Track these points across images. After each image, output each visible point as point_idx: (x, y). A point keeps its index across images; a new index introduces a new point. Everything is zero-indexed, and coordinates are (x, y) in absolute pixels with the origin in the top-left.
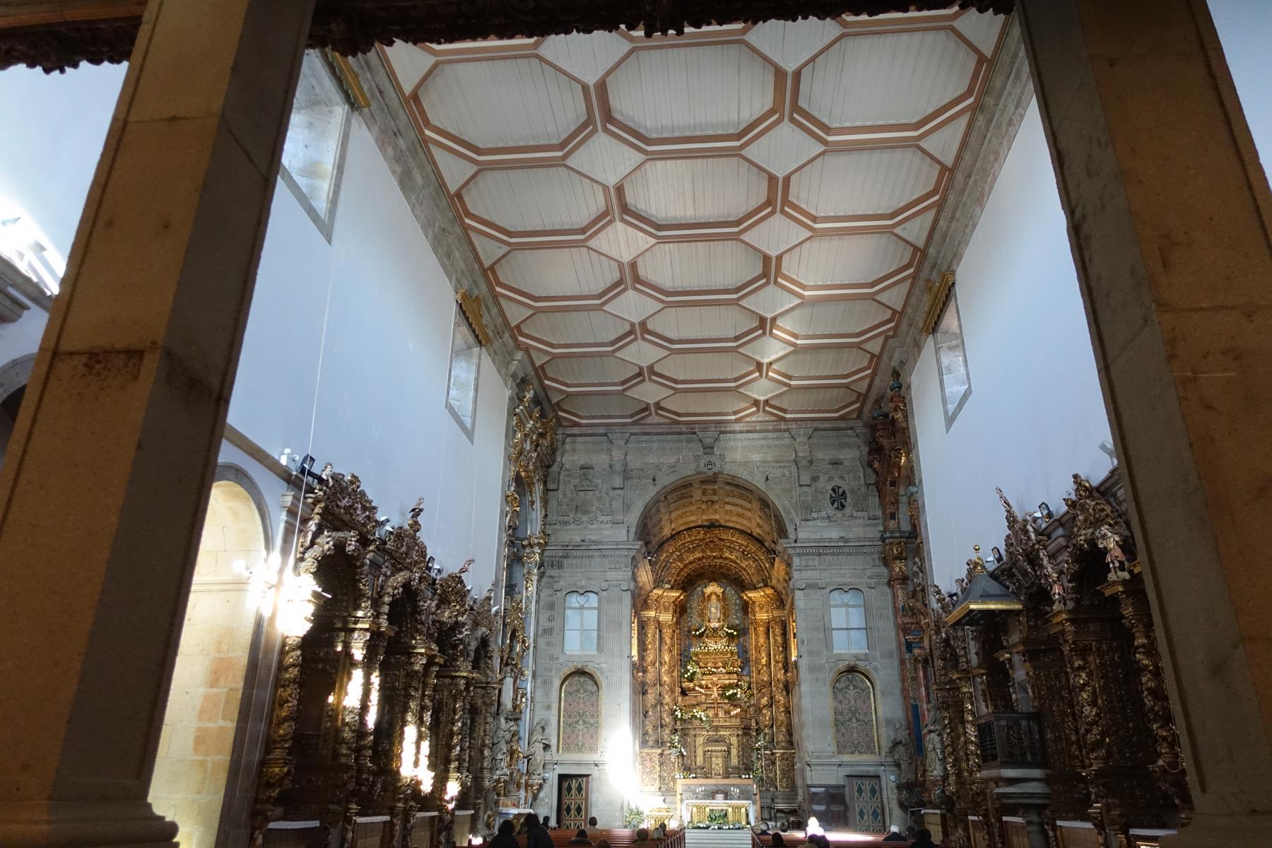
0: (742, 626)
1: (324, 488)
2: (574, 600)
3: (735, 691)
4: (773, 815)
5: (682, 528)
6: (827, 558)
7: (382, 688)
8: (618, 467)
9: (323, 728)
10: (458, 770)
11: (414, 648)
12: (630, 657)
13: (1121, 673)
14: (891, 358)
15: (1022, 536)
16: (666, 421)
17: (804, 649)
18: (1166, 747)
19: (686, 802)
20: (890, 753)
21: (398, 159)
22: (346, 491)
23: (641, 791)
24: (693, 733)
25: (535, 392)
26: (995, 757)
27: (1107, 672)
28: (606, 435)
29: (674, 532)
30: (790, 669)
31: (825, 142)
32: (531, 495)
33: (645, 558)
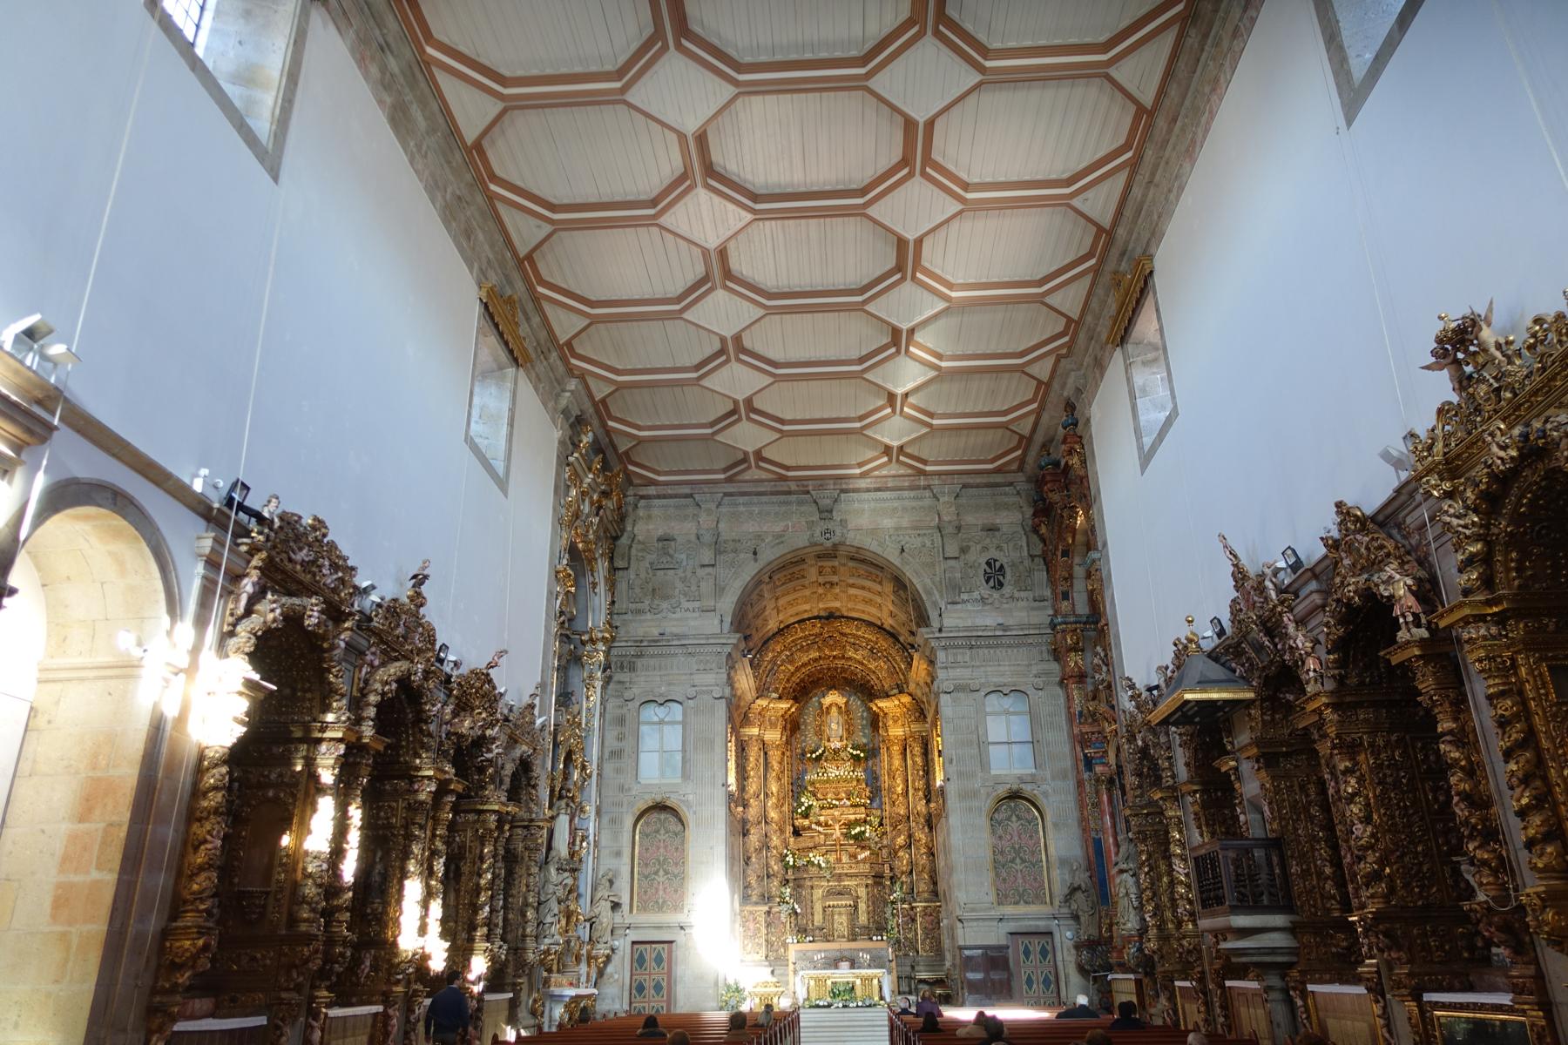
0: (871, 746)
1: (266, 531)
2: (652, 713)
3: (863, 829)
4: (913, 987)
5: (792, 620)
6: (980, 651)
7: (368, 826)
8: (707, 538)
9: (274, 880)
10: (488, 938)
11: (419, 769)
12: (725, 785)
13: (1403, 777)
14: (1063, 386)
15: (1256, 598)
16: (771, 476)
17: (952, 769)
18: (1489, 876)
19: (801, 973)
20: (1066, 901)
21: (385, 84)
22: (304, 540)
23: (742, 961)
24: (809, 884)
25: (595, 435)
26: (1220, 901)
27: (1385, 775)
28: (691, 496)
29: (782, 626)
30: (933, 798)
31: (982, 69)
32: (592, 575)
33: (745, 656)
